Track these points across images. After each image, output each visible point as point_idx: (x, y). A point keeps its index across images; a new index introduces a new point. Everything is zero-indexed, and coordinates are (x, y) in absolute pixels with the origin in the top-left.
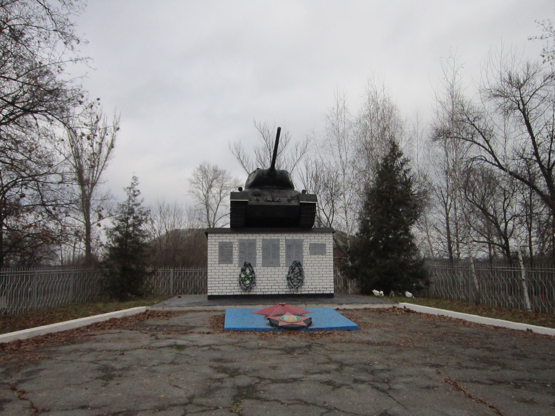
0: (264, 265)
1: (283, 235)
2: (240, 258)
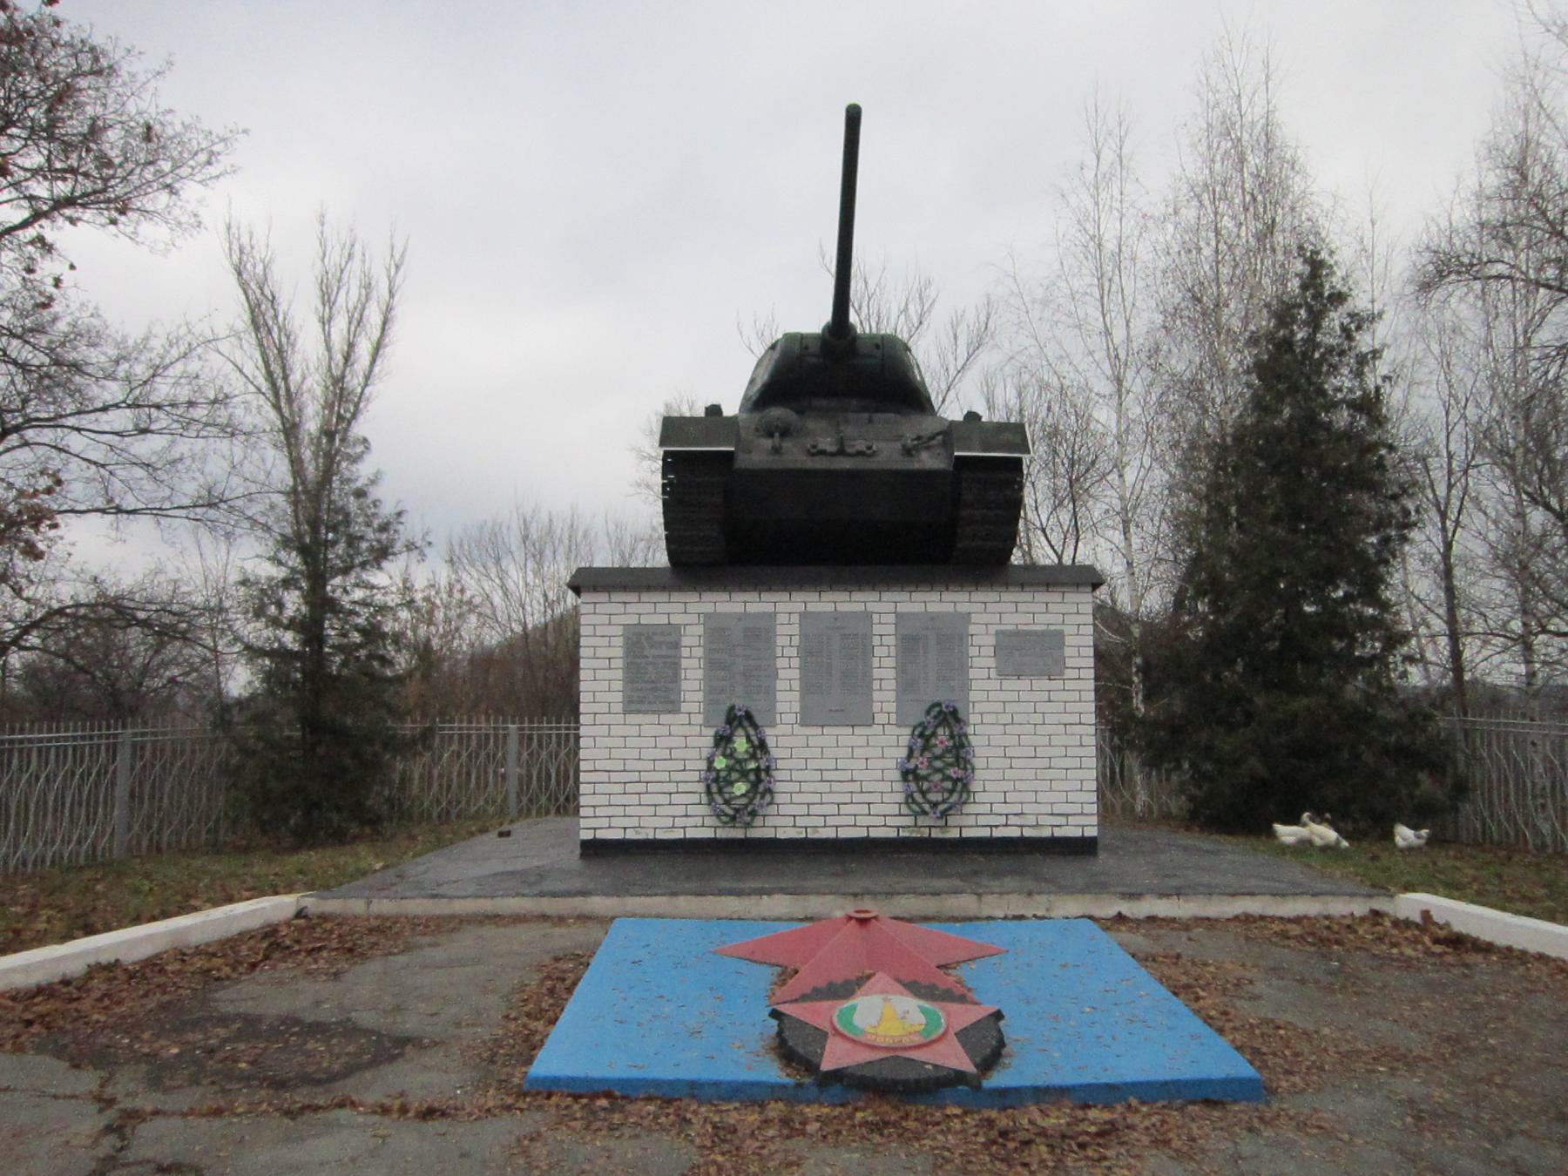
0: (807, 718)
1: (886, 596)
2: (712, 693)
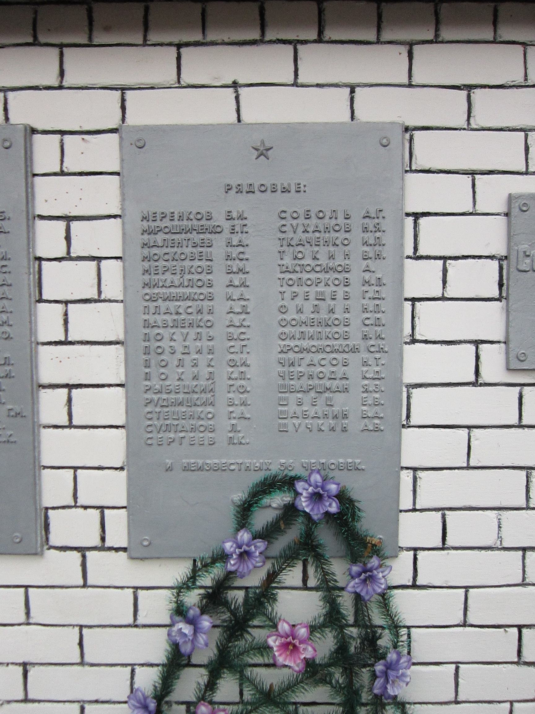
1: (84, 66)
